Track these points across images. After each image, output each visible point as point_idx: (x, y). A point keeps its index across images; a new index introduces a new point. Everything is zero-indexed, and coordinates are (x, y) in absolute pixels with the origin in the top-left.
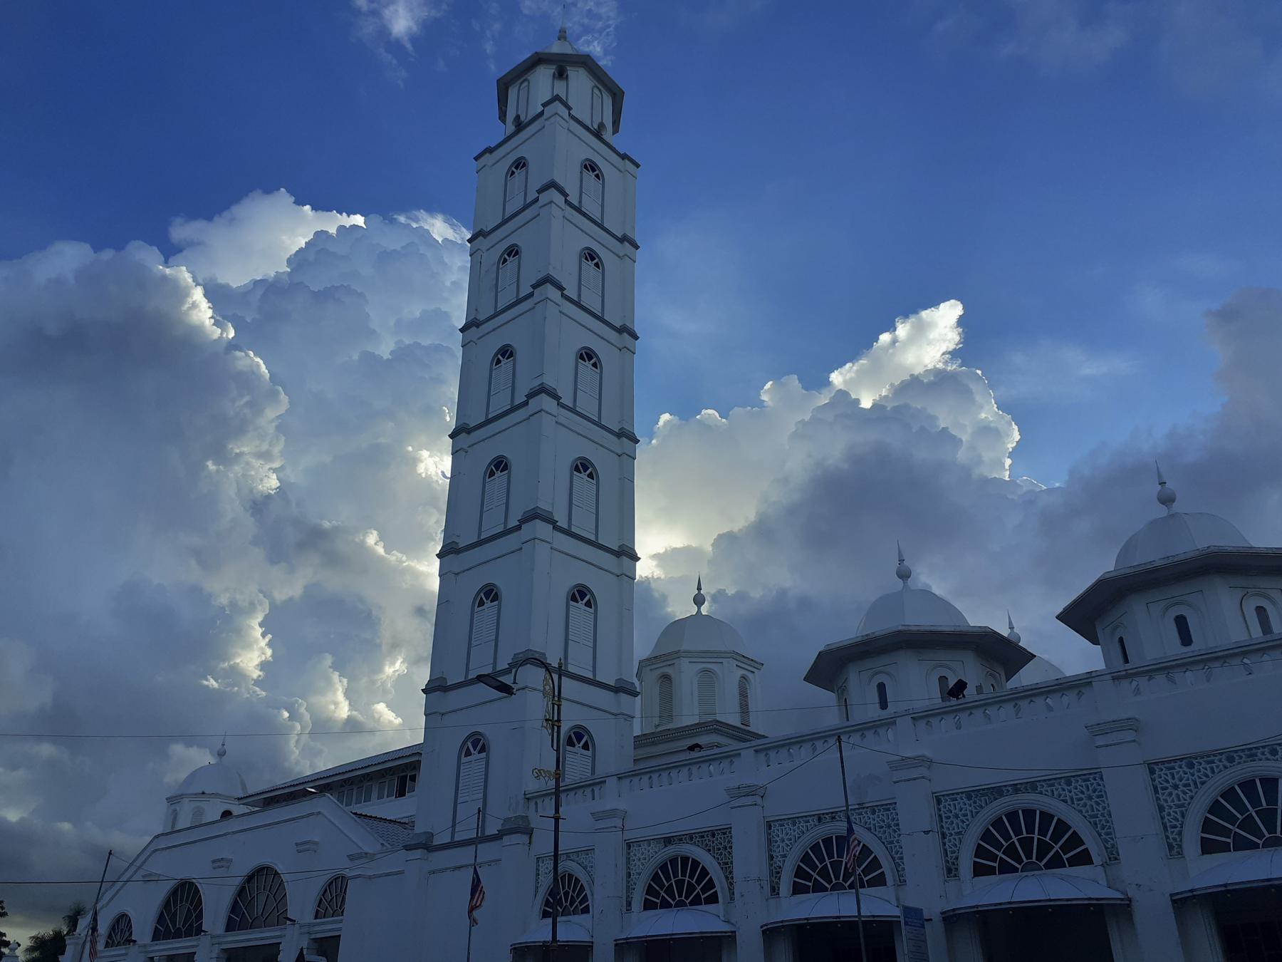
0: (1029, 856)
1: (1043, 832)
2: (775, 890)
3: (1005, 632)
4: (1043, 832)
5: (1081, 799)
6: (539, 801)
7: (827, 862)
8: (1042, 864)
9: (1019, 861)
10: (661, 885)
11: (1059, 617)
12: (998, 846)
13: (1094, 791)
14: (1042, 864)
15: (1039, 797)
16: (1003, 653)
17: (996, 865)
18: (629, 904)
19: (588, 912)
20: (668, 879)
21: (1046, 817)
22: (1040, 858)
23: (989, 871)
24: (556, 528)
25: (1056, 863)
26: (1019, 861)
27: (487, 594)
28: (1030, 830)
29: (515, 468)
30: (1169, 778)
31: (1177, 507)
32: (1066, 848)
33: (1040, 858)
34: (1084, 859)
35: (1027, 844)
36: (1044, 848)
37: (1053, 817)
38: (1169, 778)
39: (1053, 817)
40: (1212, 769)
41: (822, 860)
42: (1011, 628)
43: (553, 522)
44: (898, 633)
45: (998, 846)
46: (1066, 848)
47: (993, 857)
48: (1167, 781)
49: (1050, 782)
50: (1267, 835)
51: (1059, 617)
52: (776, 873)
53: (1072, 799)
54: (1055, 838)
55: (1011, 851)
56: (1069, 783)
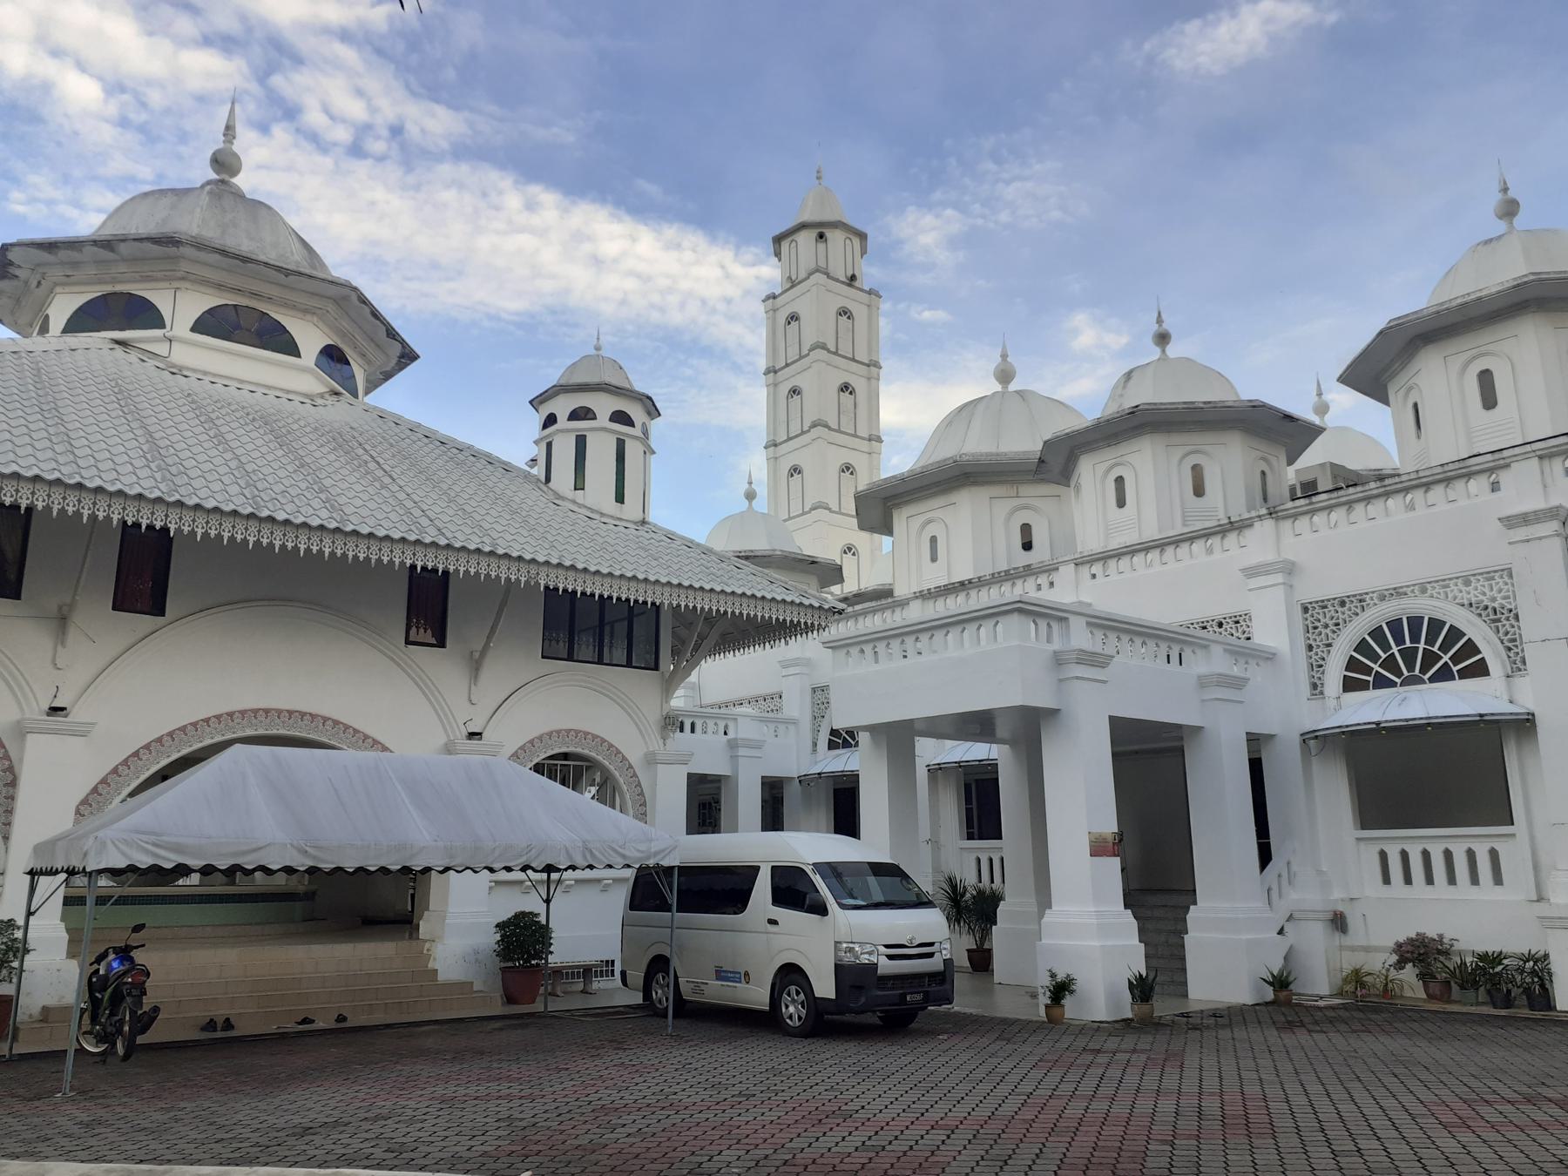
0: (1411, 668)
1: (1430, 640)
2: (1316, 687)
6: (711, 723)
9: (1399, 674)
13: (1500, 591)
18: (815, 745)
22: (1424, 670)
23: (1362, 686)
24: (829, 428)
25: (1444, 675)
26: (1399, 674)
29: (805, 393)
30: (1487, 590)
31: (1173, 350)
33: (1424, 670)
34: (1480, 670)
35: (1409, 656)
36: (1431, 657)
37: (1444, 623)
38: (1487, 590)
39: (1444, 623)
43: (829, 428)
49: (1444, 583)
52: (1317, 667)
55: (1390, 663)
56: (1467, 583)
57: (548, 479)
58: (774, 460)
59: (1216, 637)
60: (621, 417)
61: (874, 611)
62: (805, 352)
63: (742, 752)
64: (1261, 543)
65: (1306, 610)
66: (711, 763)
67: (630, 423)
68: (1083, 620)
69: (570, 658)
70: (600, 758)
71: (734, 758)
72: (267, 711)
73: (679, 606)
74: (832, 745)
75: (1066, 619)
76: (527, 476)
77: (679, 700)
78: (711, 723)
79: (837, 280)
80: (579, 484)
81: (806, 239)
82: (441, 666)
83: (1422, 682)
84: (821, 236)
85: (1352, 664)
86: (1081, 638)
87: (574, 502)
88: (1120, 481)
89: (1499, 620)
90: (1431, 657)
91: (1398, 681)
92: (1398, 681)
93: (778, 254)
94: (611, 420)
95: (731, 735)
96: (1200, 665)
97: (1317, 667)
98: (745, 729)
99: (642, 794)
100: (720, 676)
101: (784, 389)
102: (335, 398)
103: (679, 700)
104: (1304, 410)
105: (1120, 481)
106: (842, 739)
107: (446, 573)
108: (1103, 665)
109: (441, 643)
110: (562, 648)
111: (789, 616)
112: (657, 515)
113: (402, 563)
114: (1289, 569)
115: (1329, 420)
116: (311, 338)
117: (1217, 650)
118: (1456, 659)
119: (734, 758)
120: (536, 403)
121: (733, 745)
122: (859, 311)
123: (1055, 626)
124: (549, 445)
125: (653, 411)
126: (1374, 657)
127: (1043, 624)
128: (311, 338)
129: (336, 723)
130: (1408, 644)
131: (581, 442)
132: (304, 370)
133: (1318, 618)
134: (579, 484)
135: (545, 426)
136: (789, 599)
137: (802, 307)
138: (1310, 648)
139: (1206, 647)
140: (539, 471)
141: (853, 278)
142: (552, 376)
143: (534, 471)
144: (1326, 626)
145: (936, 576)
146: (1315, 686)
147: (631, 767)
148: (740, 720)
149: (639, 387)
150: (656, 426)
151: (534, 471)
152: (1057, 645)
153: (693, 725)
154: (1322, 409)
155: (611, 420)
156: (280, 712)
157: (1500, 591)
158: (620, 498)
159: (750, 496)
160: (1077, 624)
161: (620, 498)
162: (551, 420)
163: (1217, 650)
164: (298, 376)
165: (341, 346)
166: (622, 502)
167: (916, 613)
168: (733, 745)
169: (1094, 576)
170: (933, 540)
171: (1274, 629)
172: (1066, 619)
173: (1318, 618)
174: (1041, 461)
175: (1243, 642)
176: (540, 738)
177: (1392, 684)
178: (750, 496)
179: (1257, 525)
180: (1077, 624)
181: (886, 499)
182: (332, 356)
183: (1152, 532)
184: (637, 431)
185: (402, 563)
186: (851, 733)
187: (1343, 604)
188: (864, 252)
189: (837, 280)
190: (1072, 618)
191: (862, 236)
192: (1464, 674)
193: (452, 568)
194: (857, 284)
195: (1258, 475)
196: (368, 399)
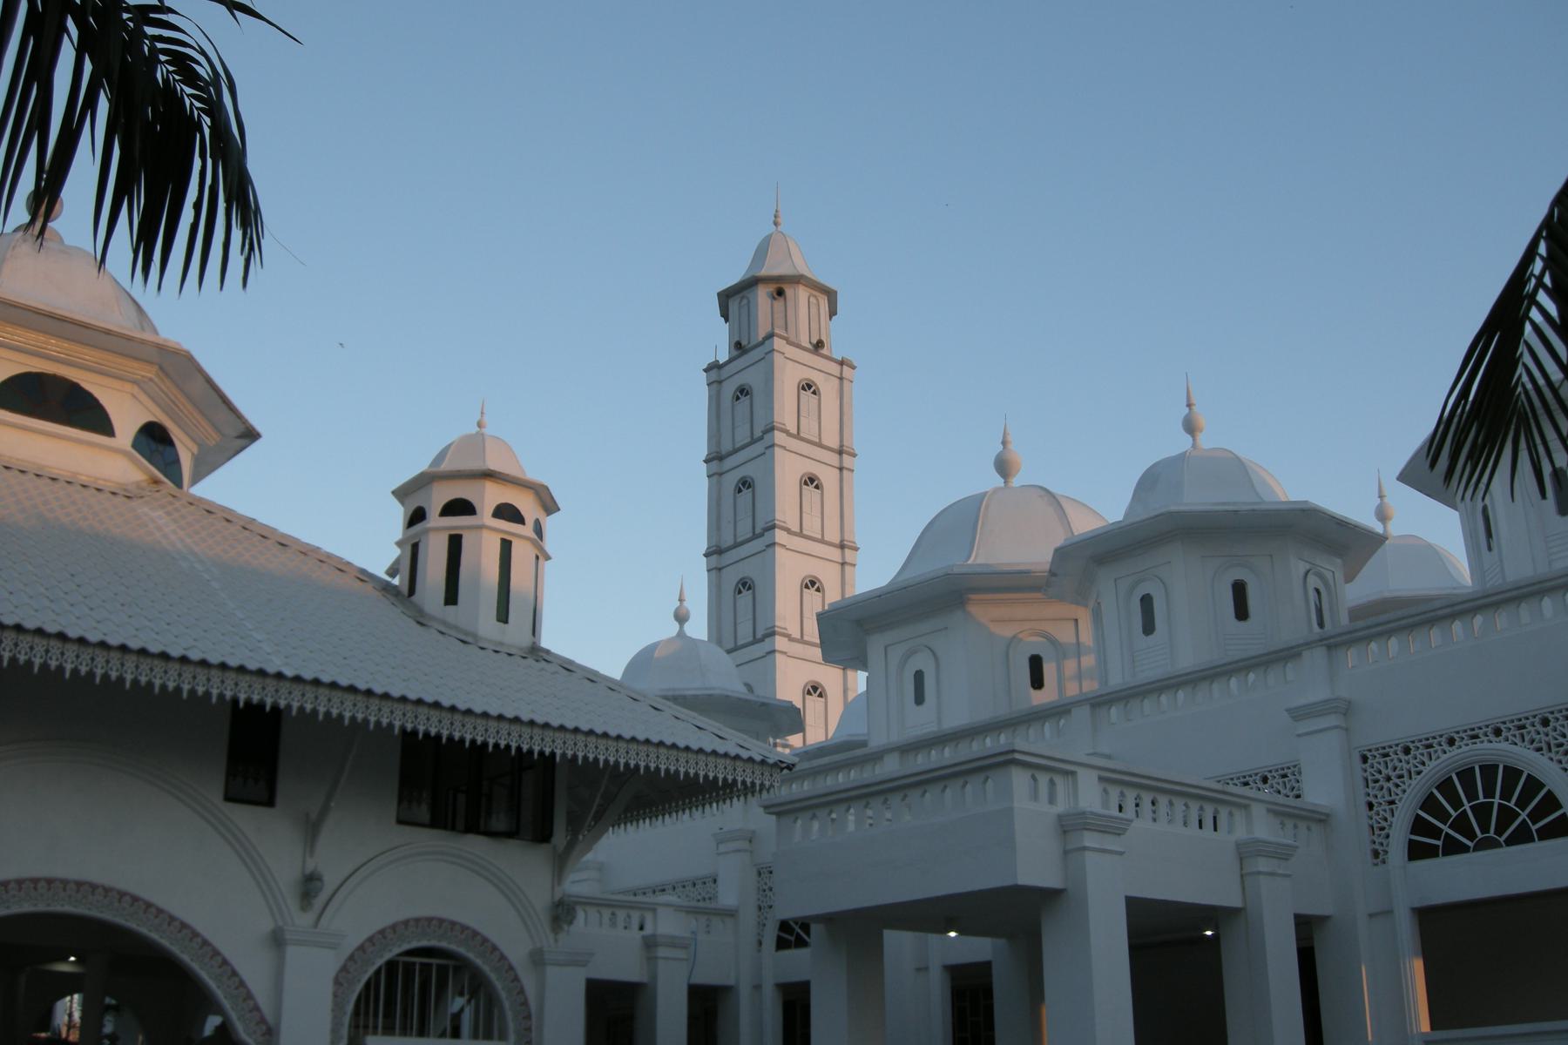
0: (1485, 829)
5: (1376, 781)
6: (621, 914)
7: (1467, 806)
9: (1470, 835)
15: (1504, 746)
16: (1343, 542)
17: (1439, 843)
19: (784, 926)
21: (1512, 774)
22: (1499, 832)
26: (1470, 835)
27: (744, 584)
30: (1382, 768)
33: (1499, 832)
35: (1482, 812)
36: (1507, 816)
41: (1456, 804)
47: (1435, 833)
50: (1492, 833)
52: (1380, 830)
55: (1462, 825)
57: (412, 591)
58: (715, 571)
59: (1260, 795)
60: (507, 512)
61: (45, 332)
63: (662, 952)
64: (1309, 681)
65: (1365, 759)
66: (623, 966)
68: (1094, 774)
70: (471, 956)
71: (651, 960)
73: (575, 757)
74: (782, 944)
75: (1073, 773)
76: (386, 588)
77: (578, 883)
78: (621, 914)
80: (451, 597)
82: (270, 834)
83: (1498, 845)
84: (780, 293)
85: (1419, 826)
86: (1090, 796)
87: (445, 623)
88: (1147, 601)
90: (1507, 816)
91: (1470, 844)
92: (1470, 844)
93: (725, 315)
95: (648, 930)
96: (1238, 829)
97: (1380, 830)
98: (668, 924)
99: (525, 1003)
100: (629, 853)
101: (731, 480)
102: (155, 487)
103: (578, 883)
104: (1365, 518)
105: (1147, 601)
106: (791, 935)
107: (275, 708)
108: (1119, 832)
110: (424, 813)
111: (720, 771)
112: (547, 641)
113: (221, 696)
114: (1345, 709)
115: (1395, 529)
117: (1258, 811)
118: (1535, 816)
119: (651, 960)
120: (402, 494)
121: (650, 944)
122: (827, 387)
123: (1059, 780)
125: (550, 506)
126: (1443, 816)
127: (1043, 779)
129: (135, 899)
133: (1377, 767)
134: (451, 597)
136: (721, 750)
138: (1371, 806)
139: (1246, 807)
141: (819, 345)
142: (419, 464)
144: (1388, 779)
145: (922, 721)
146: (1376, 854)
147: (511, 968)
148: (660, 910)
149: (533, 474)
151: (396, 581)
152: (1061, 807)
154: (1382, 515)
156: (65, 882)
159: (681, 617)
162: (417, 517)
163: (1258, 811)
164: (110, 461)
166: (506, 621)
167: (891, 767)
168: (650, 944)
170: (919, 677)
171: (1328, 785)
172: (1073, 773)
174: (1052, 573)
175: (1292, 801)
176: (394, 927)
177: (1465, 849)
178: (681, 617)
179: (1306, 654)
181: (859, 623)
182: (154, 439)
183: (1188, 659)
184: (527, 530)
185: (221, 696)
186: (805, 927)
188: (833, 312)
189: (799, 346)
190: (1081, 771)
191: (831, 295)
192: (1545, 834)
193: (282, 703)
194: (824, 351)
195: (1312, 595)
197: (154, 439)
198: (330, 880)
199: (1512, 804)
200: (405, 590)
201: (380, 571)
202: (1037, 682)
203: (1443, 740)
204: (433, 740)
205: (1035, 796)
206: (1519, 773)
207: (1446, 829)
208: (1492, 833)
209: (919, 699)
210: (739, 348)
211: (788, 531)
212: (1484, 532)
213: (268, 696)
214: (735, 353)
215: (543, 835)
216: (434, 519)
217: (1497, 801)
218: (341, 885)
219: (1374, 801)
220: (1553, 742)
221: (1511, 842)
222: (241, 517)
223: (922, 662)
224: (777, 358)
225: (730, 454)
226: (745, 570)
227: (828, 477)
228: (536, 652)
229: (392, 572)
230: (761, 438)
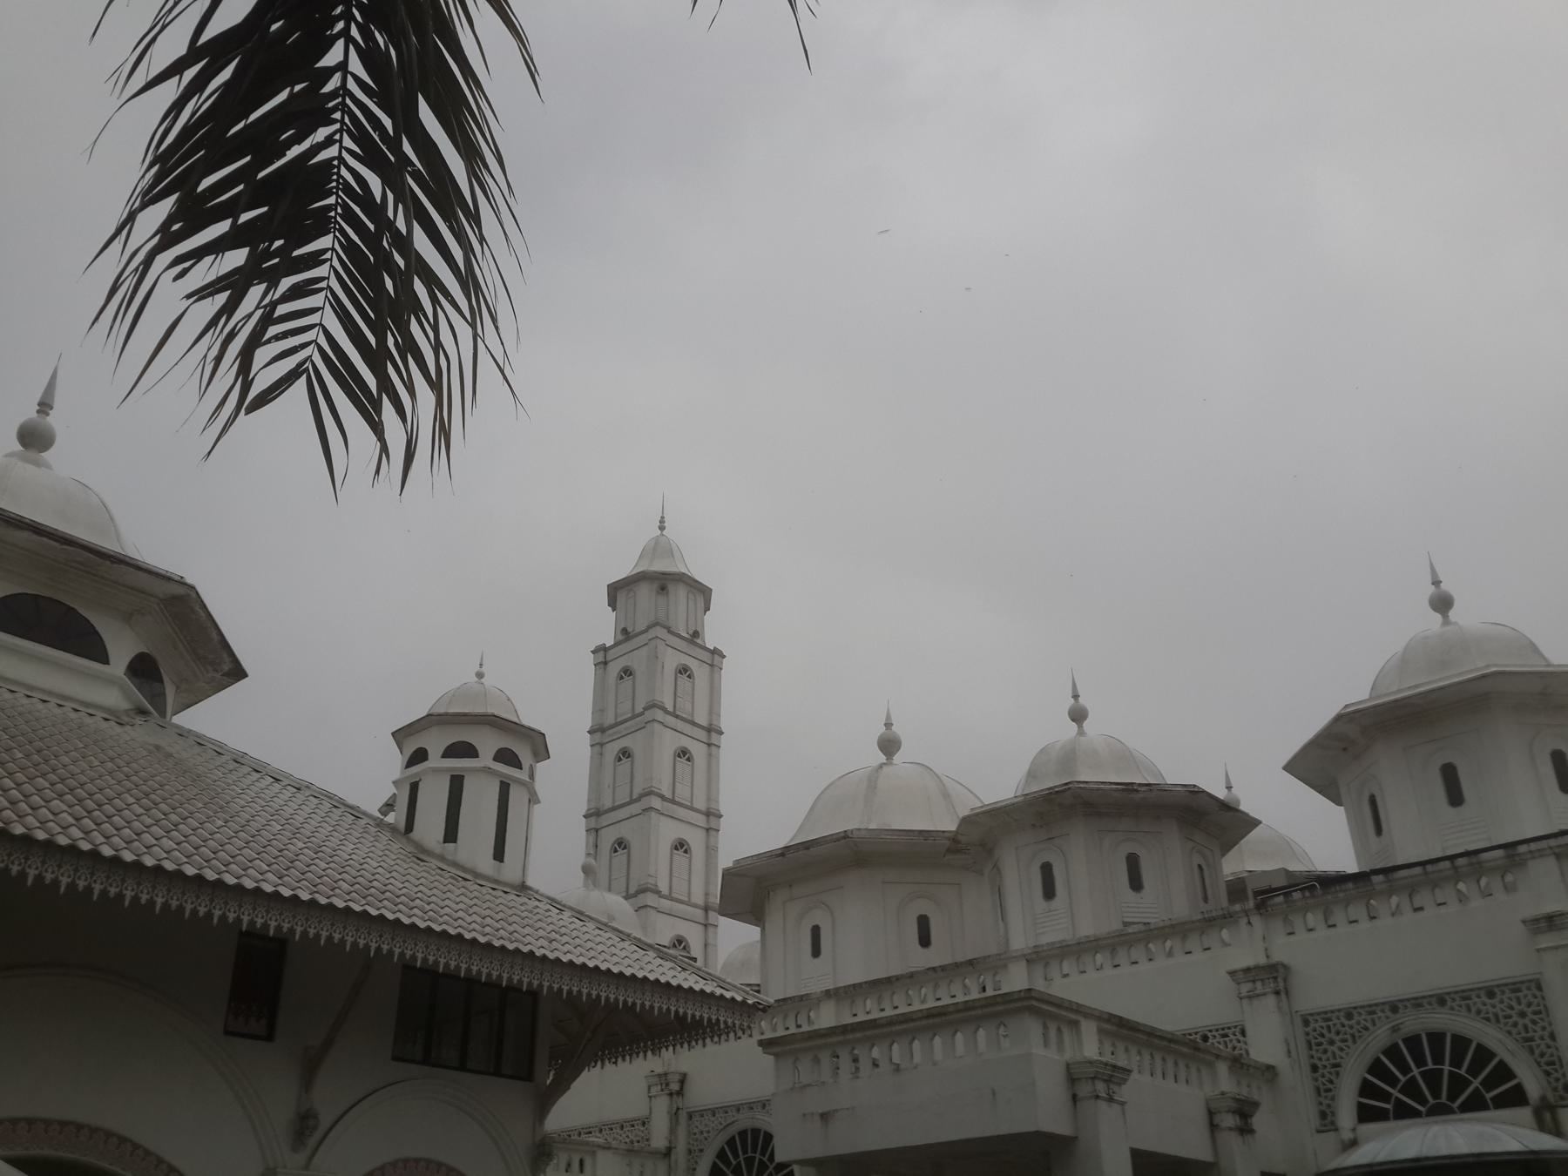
0: (1436, 1095)
1: (1456, 1062)
2: (1326, 1120)
3: (1220, 793)
4: (1456, 1062)
5: (1319, 1044)
8: (1456, 1105)
9: (1423, 1101)
10: (728, 1164)
11: (1290, 767)
12: (1393, 1081)
13: (1529, 1005)
14: (1456, 1105)
16: (1208, 819)
20: (736, 1156)
21: (1461, 1042)
23: (1381, 1116)
26: (1423, 1101)
27: (620, 844)
28: (1438, 1059)
30: (1514, 1003)
32: (1489, 1084)
33: (1453, 1097)
35: (1433, 1078)
38: (1514, 1003)
40: (1518, 999)
42: (1229, 788)
44: (1129, 788)
45: (1393, 1081)
46: (1489, 1084)
47: (1385, 1097)
48: (1512, 1008)
49: (1465, 995)
51: (1290, 767)
53: (1496, 1016)
54: (1474, 1070)
55: (1411, 1089)
62: (639, 709)
64: (1246, 946)
65: (1306, 1023)
67: (518, 765)
69: (426, 1061)
72: (30, 1121)
76: (380, 824)
79: (679, 636)
80: (451, 834)
81: (645, 592)
84: (663, 588)
85: (1366, 1089)
86: (1090, 1046)
89: (1531, 1039)
90: (1458, 1084)
93: (612, 603)
94: (497, 758)
97: (1325, 1092)
109: (269, 1037)
112: (529, 883)
116: (122, 647)
120: (400, 736)
123: (1065, 1030)
124: (414, 787)
128: (122, 647)
130: (1431, 1066)
131: (457, 784)
132: (110, 681)
134: (451, 834)
135: (410, 763)
137: (638, 661)
138: (1314, 1068)
140: (395, 818)
141: (696, 634)
143: (390, 818)
144: (1332, 1042)
146: (1323, 1115)
150: (541, 767)
151: (390, 818)
152: (1068, 1055)
153: (581, 1162)
155: (497, 758)
157: (1529, 1005)
158: (499, 855)
160: (1089, 1029)
161: (499, 855)
162: (419, 756)
164: (103, 687)
165: (154, 654)
167: (827, 1017)
169: (1065, 976)
173: (1322, 1034)
180: (1089, 1029)
183: (1087, 928)
184: (522, 775)
187: (1349, 1016)
188: (707, 609)
189: (679, 636)
195: (1196, 869)
196: (177, 719)
197: (144, 670)
198: (325, 1120)
199: (1463, 1072)
200: (402, 825)
201: (373, 808)
202: (925, 941)
203: (1449, 1003)
204: (430, 973)
205: (1046, 1044)
206: (1468, 1041)
207: (1395, 1092)
208: (1444, 1098)
209: (816, 952)
210: (625, 635)
211: (663, 797)
212: (1372, 819)
213: (273, 922)
214: (620, 637)
215: (526, 1073)
216: (435, 760)
217: (1416, 1072)
218: (336, 1122)
219: (1319, 1064)
220: (1501, 1014)
221: (1465, 1108)
222: (231, 751)
223: (819, 917)
224: (661, 646)
225: (612, 727)
226: (624, 831)
227: (698, 750)
228: (523, 888)
229: (389, 806)
230: (642, 714)
